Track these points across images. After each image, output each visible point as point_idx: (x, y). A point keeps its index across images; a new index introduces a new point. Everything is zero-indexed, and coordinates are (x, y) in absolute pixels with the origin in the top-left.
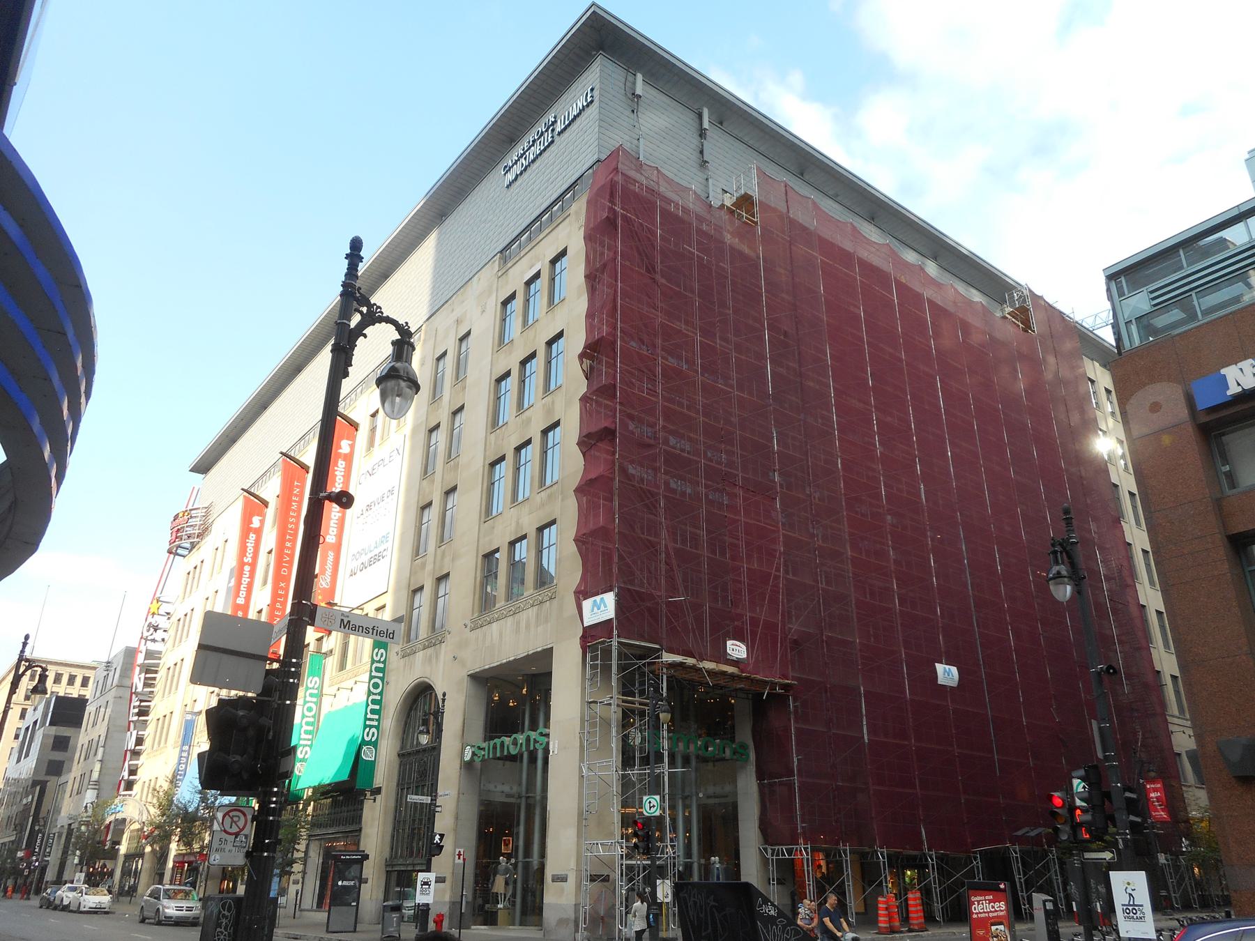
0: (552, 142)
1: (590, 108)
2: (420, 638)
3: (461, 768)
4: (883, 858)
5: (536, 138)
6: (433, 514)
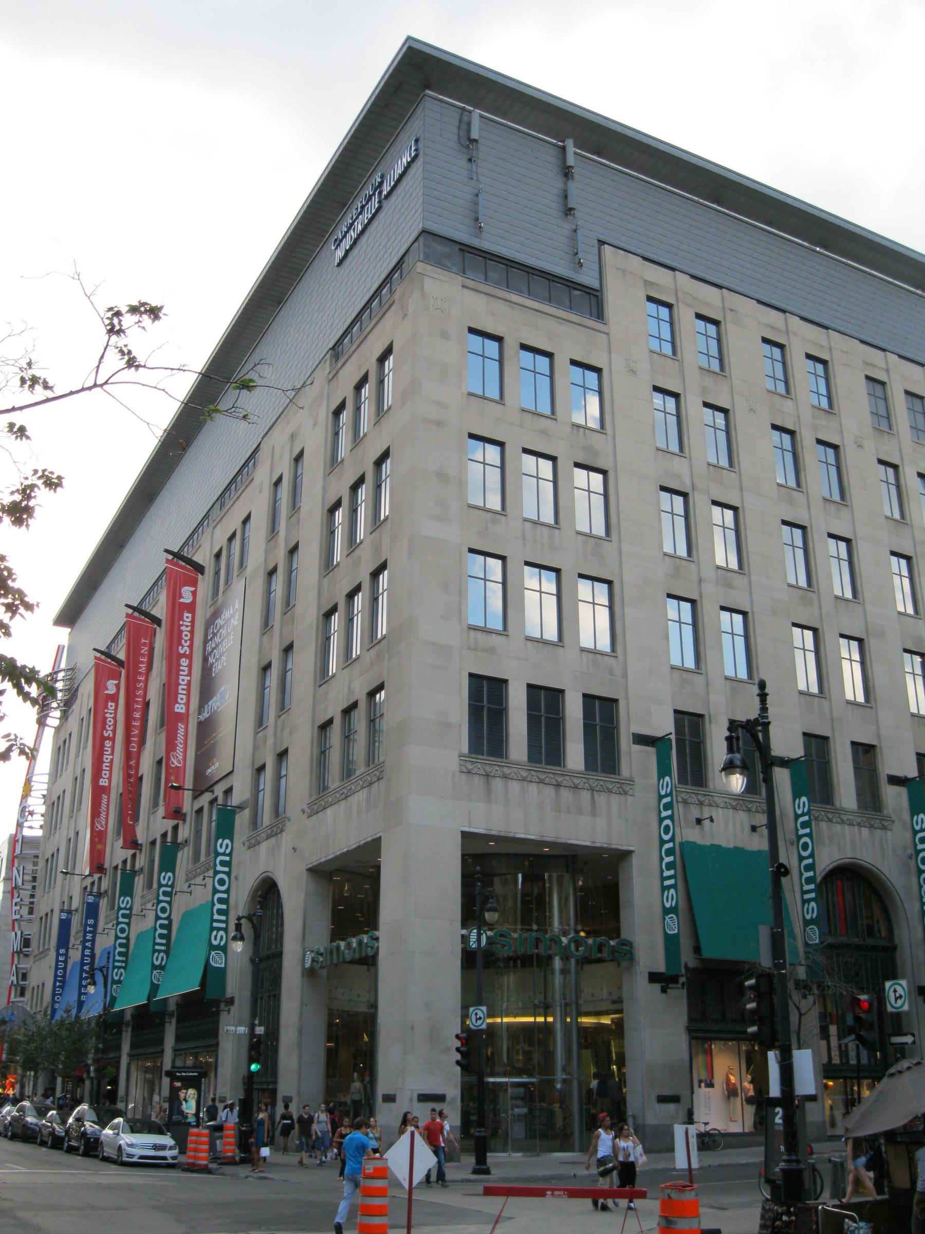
2: (264, 826)
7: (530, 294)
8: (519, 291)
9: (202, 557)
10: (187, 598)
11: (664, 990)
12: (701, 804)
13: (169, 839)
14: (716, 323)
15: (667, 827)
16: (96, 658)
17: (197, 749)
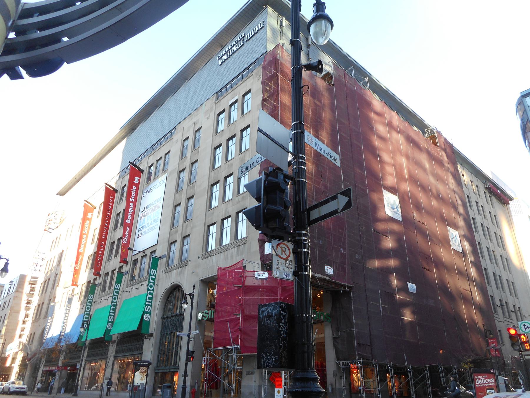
0: (243, 45)
1: (232, 56)
2: (175, 264)
3: (196, 323)
4: (391, 367)
5: (235, 43)
9: (143, 166)
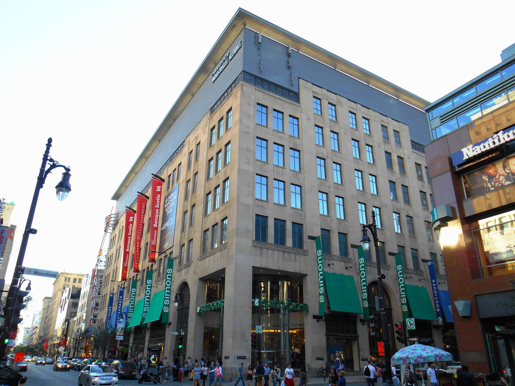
0: (228, 64)
6: (188, 214)
7: (276, 93)
8: (273, 92)
10: (159, 190)
11: (318, 321)
12: (330, 259)
13: (150, 269)
14: (335, 106)
15: (320, 267)
16: (126, 209)
17: (160, 240)
